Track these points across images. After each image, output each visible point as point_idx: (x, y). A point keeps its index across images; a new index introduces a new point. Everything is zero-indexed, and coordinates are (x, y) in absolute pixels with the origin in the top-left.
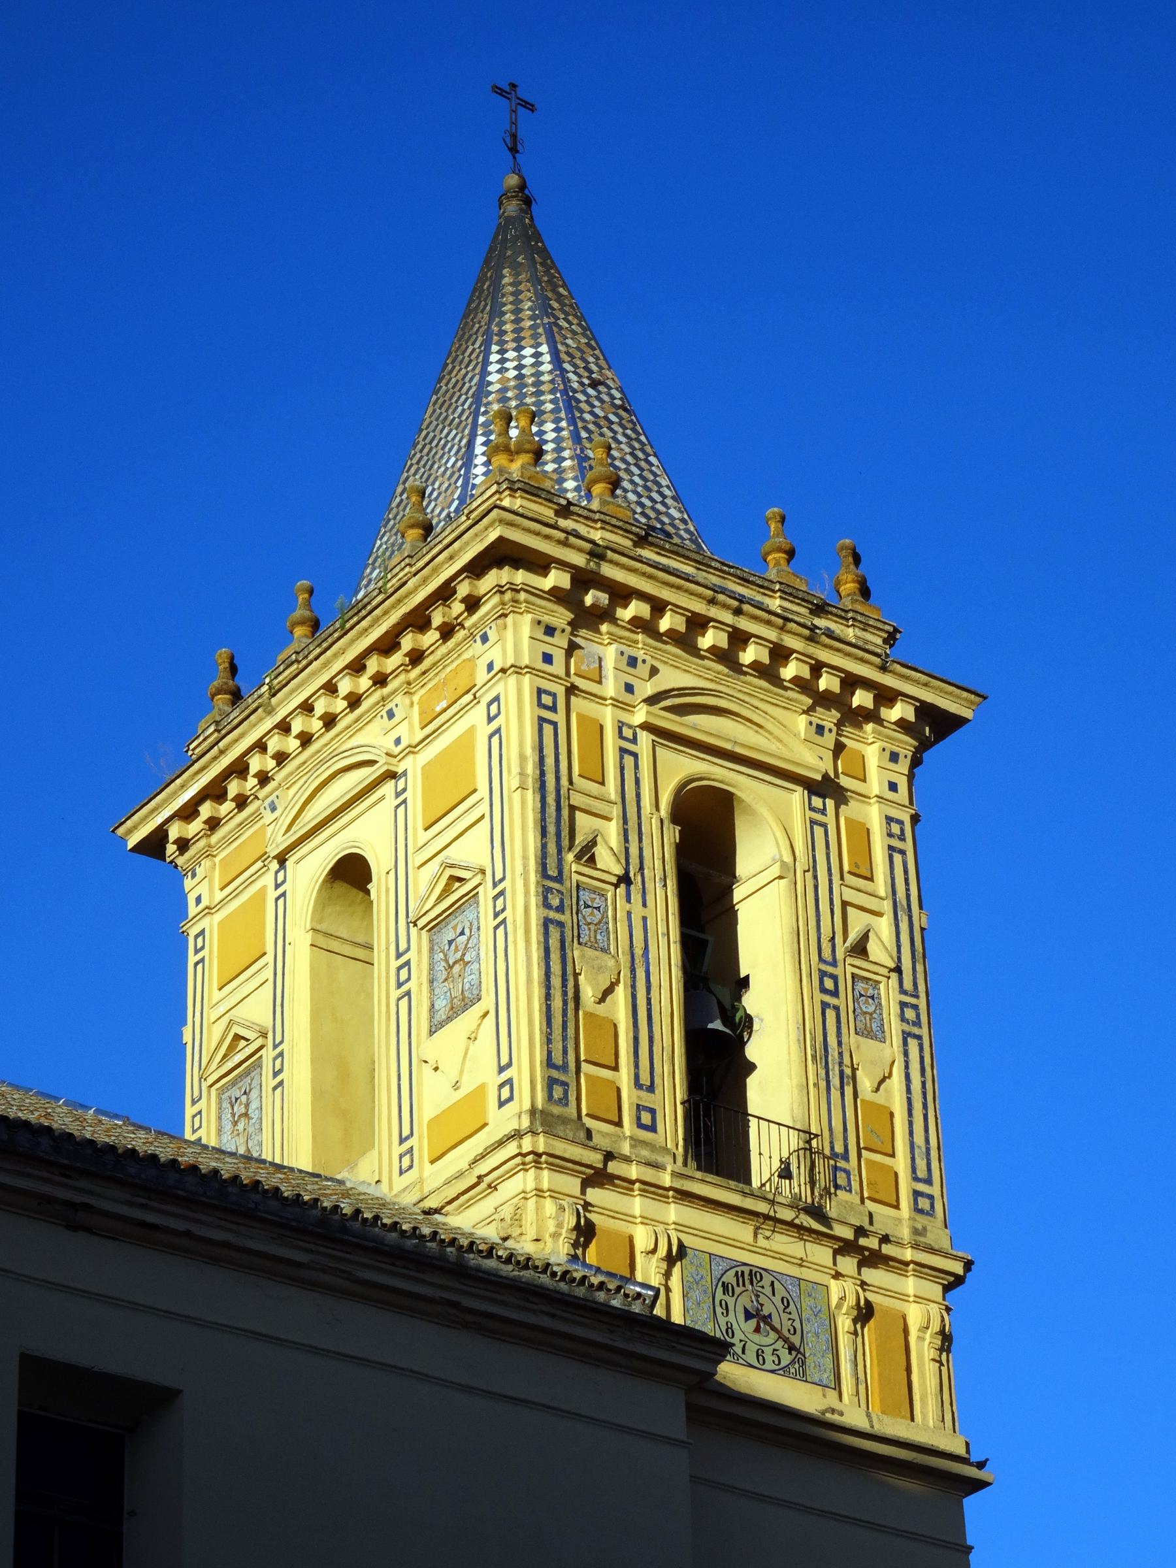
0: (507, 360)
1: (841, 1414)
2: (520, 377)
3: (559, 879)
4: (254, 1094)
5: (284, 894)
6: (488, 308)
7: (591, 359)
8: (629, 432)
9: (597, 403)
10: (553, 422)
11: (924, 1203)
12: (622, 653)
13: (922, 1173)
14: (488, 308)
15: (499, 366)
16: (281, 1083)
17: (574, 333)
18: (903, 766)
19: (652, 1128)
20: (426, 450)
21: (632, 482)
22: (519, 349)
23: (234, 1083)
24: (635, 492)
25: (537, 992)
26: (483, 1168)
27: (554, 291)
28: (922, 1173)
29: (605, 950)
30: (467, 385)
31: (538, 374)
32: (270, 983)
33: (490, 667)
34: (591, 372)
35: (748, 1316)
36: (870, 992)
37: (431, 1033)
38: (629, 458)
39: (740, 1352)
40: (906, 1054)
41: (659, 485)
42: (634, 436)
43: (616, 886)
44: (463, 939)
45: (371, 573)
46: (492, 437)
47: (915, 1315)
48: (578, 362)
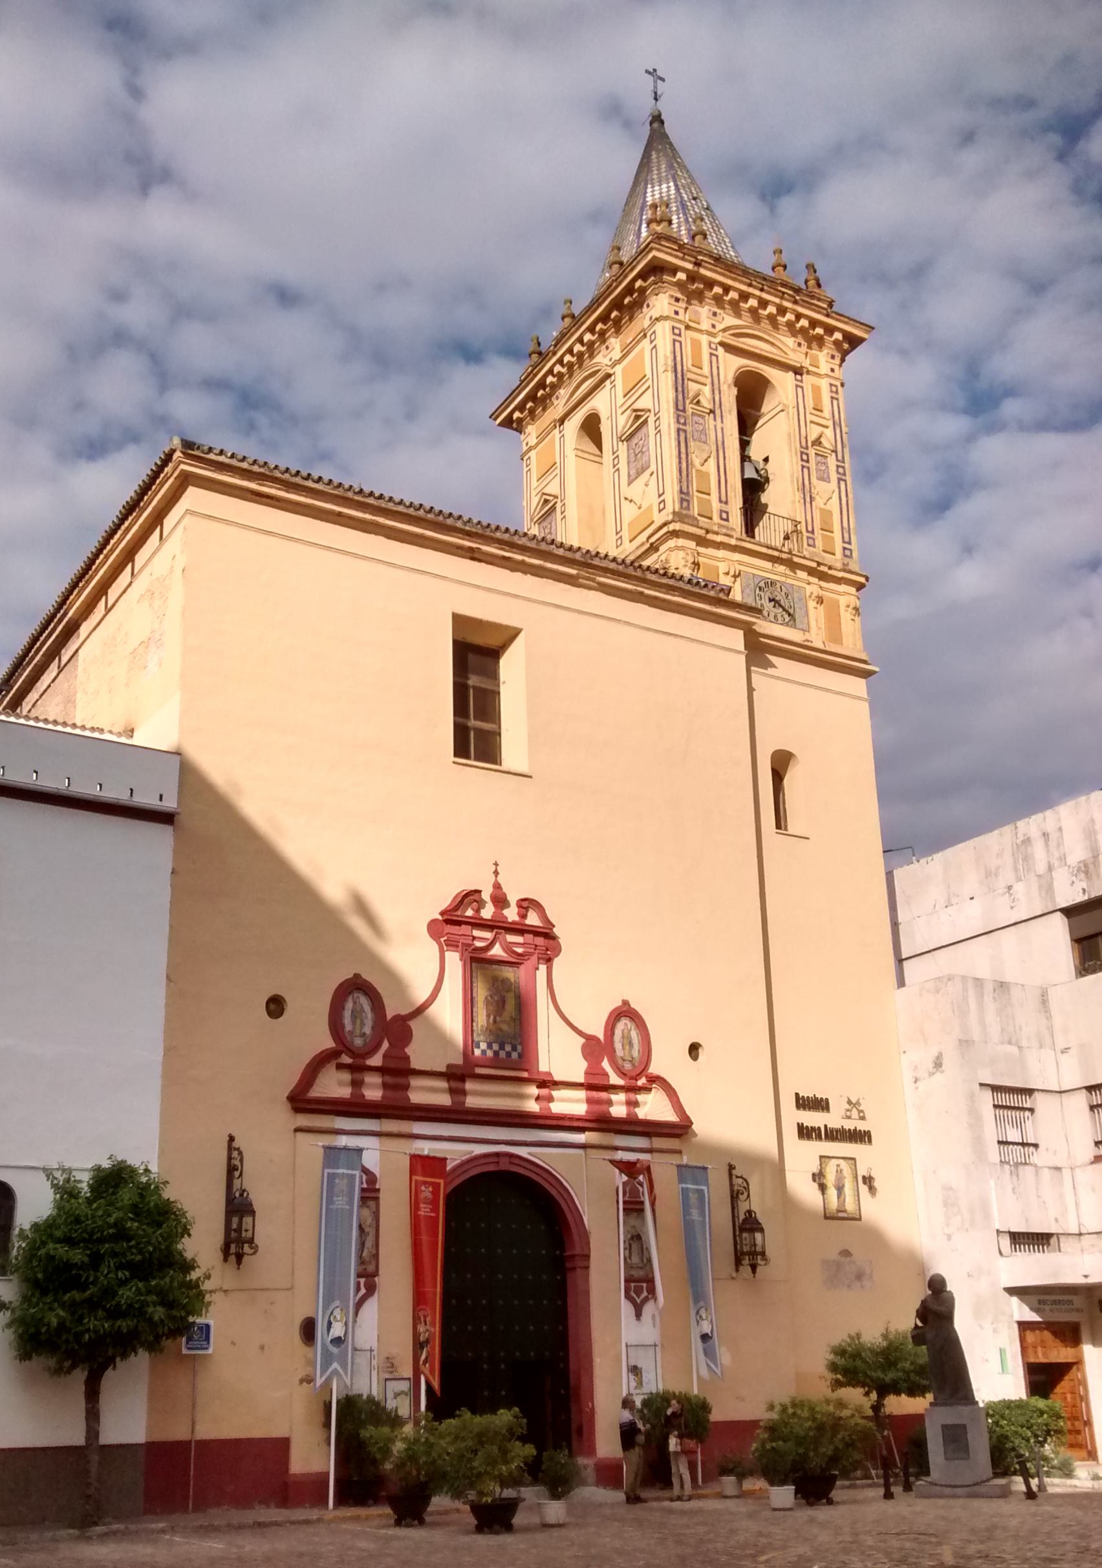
1: (812, 642)
3: (684, 410)
4: (553, 524)
11: (847, 552)
13: (847, 539)
16: (565, 517)
18: (837, 361)
22: (660, 185)
25: (675, 461)
26: (652, 540)
27: (676, 160)
28: (847, 539)
29: (705, 443)
33: (651, 318)
34: (693, 194)
35: (770, 600)
36: (823, 461)
37: (629, 485)
40: (839, 488)
41: (725, 242)
43: (709, 414)
47: (843, 601)
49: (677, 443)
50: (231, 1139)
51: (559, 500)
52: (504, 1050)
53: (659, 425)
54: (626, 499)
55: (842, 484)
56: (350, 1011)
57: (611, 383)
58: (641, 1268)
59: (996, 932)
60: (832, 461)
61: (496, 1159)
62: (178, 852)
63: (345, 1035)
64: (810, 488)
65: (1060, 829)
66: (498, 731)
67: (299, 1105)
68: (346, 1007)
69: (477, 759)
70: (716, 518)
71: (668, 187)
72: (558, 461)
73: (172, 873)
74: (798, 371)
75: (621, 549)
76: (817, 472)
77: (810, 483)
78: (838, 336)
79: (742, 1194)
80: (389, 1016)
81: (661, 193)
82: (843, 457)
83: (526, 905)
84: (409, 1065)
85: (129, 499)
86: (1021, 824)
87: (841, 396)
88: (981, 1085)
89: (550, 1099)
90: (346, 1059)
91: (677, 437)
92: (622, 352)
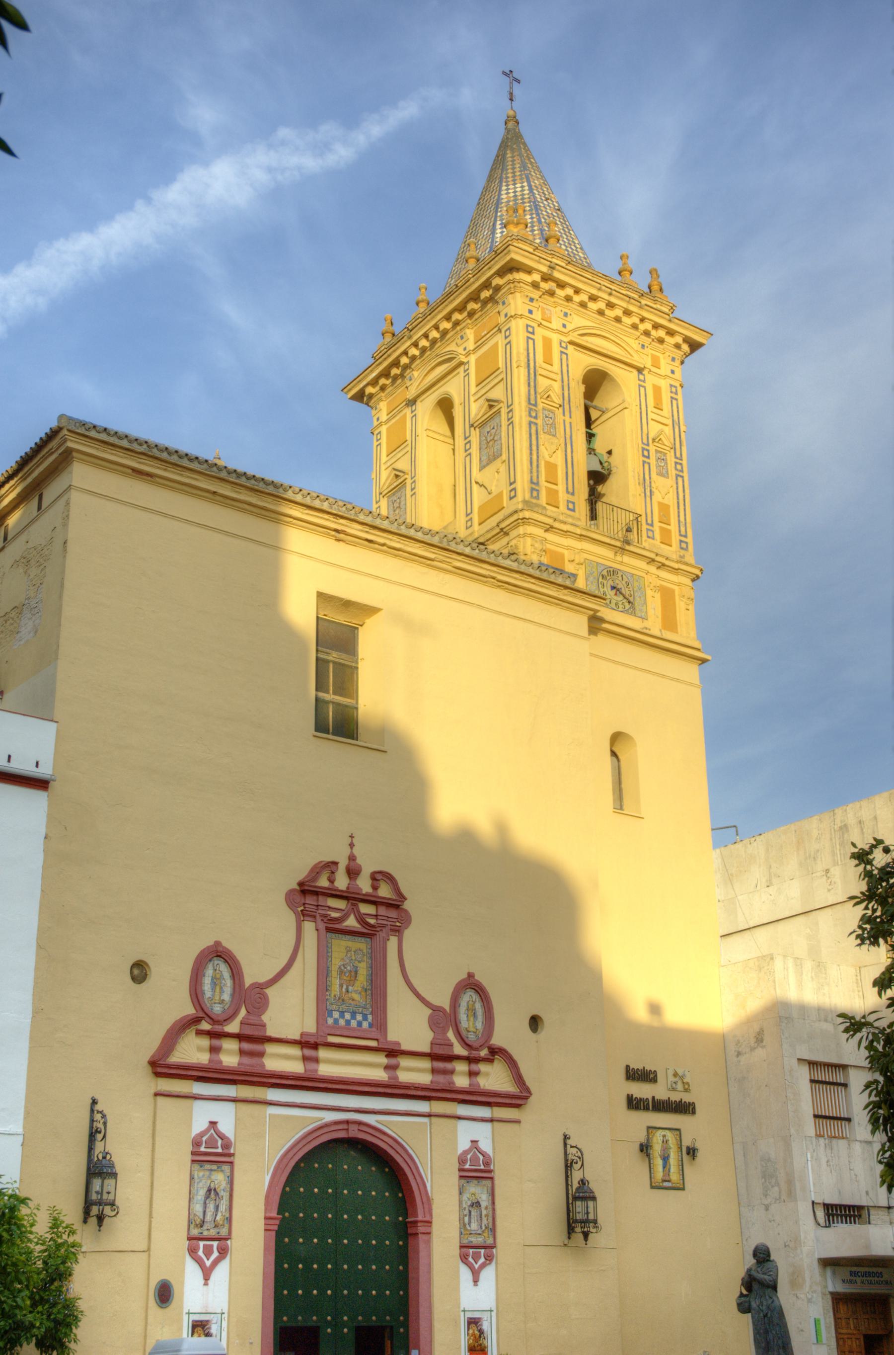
0: (509, 189)
1: (650, 630)
2: (515, 196)
3: (535, 405)
4: (403, 499)
5: (415, 415)
6: (501, 167)
7: (545, 189)
8: (562, 220)
9: (548, 208)
10: (530, 215)
11: (684, 545)
12: (561, 311)
13: (683, 533)
14: (501, 167)
15: (506, 192)
16: (414, 493)
17: (538, 178)
18: (677, 363)
19: (573, 510)
20: (474, 229)
21: (563, 241)
22: (514, 184)
23: (394, 494)
24: (565, 245)
28: (683, 533)
29: (555, 436)
30: (492, 200)
31: (523, 195)
32: (410, 452)
33: (506, 315)
34: (545, 194)
38: (562, 231)
39: (609, 603)
40: (677, 483)
41: (574, 243)
42: (563, 222)
44: (494, 430)
45: (451, 281)
46: (504, 221)
48: (540, 190)
49: (528, 436)
50: (94, 1102)
51: (408, 477)
52: (332, 1017)
53: (512, 417)
54: (477, 483)
55: (680, 480)
56: (210, 978)
57: (465, 371)
58: (479, 1234)
59: (814, 912)
60: (671, 459)
61: (345, 1126)
62: (52, 819)
63: (204, 1002)
64: (650, 482)
65: (875, 818)
66: (356, 706)
67: (160, 1070)
68: (207, 975)
69: (334, 734)
70: (563, 507)
71: (522, 187)
72: (408, 437)
73: (46, 838)
74: (640, 370)
75: (470, 530)
76: (657, 468)
77: (650, 478)
78: (679, 339)
79: (576, 1163)
80: (247, 984)
81: (515, 192)
82: (681, 455)
83: (377, 877)
84: (265, 1031)
85: (9, 469)
86: (839, 812)
87: (680, 397)
88: (799, 1059)
89: (316, 1060)
90: (205, 1026)
91: (528, 430)
92: (475, 343)
